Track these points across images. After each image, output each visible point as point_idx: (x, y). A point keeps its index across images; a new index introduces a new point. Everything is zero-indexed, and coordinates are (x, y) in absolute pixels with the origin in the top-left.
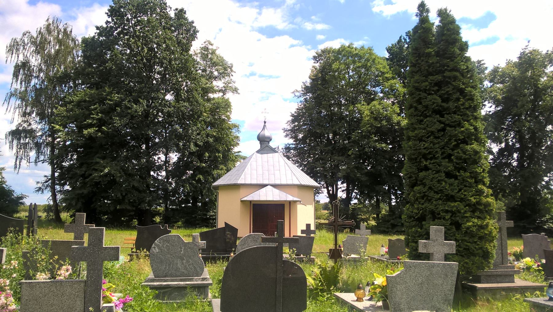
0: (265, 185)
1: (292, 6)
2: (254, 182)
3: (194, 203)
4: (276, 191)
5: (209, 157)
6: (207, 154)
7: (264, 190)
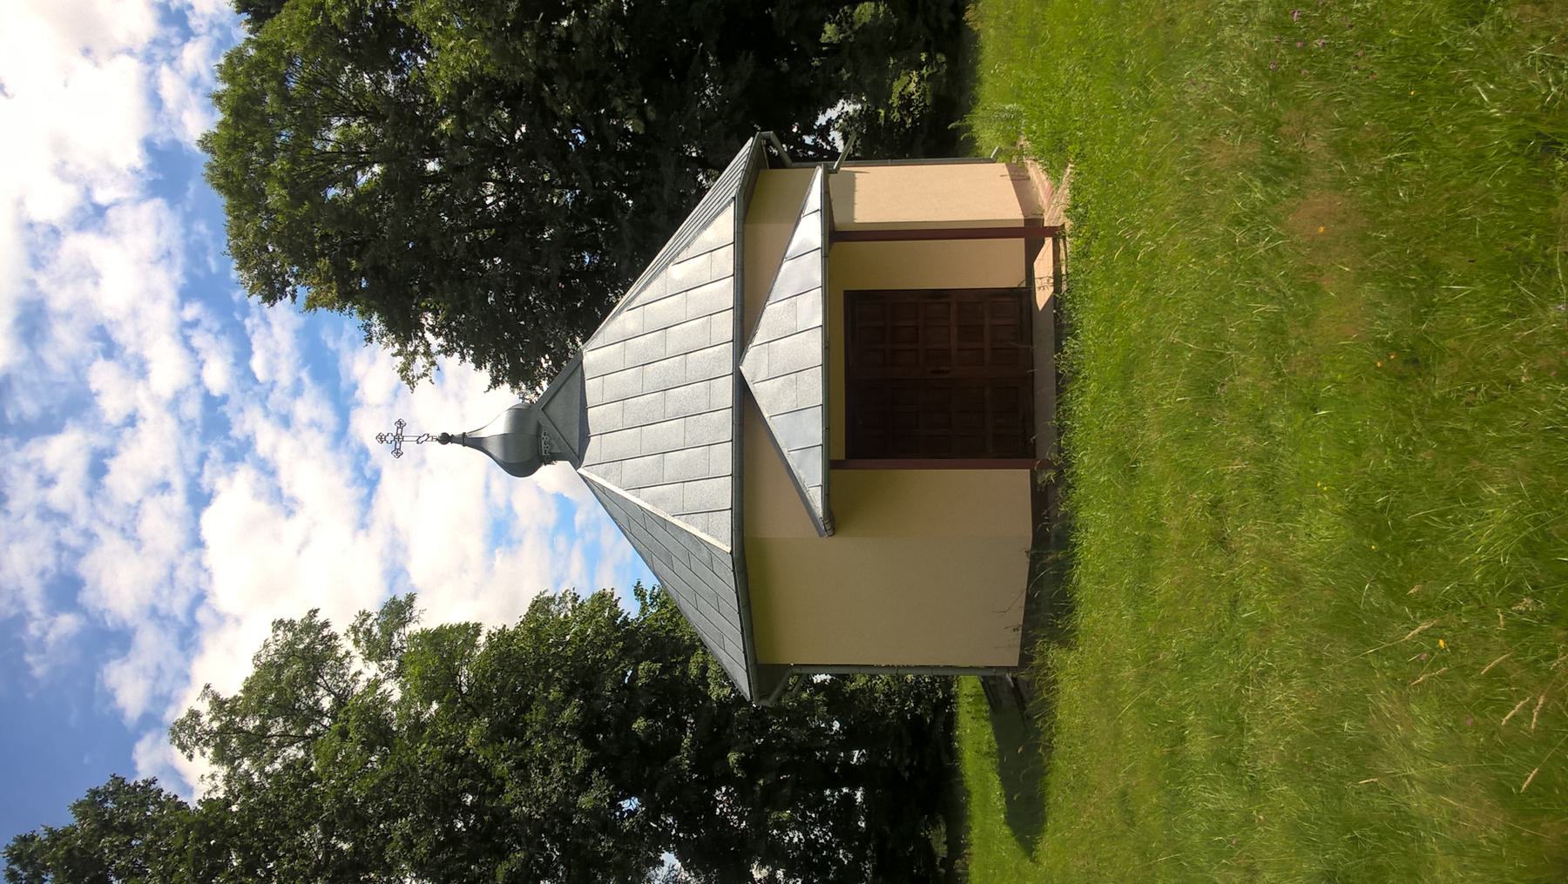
0: (743, 393)
1: (69, 423)
2: (723, 457)
3: (853, 776)
4: (773, 315)
5: (650, 714)
6: (639, 724)
7: (763, 393)
